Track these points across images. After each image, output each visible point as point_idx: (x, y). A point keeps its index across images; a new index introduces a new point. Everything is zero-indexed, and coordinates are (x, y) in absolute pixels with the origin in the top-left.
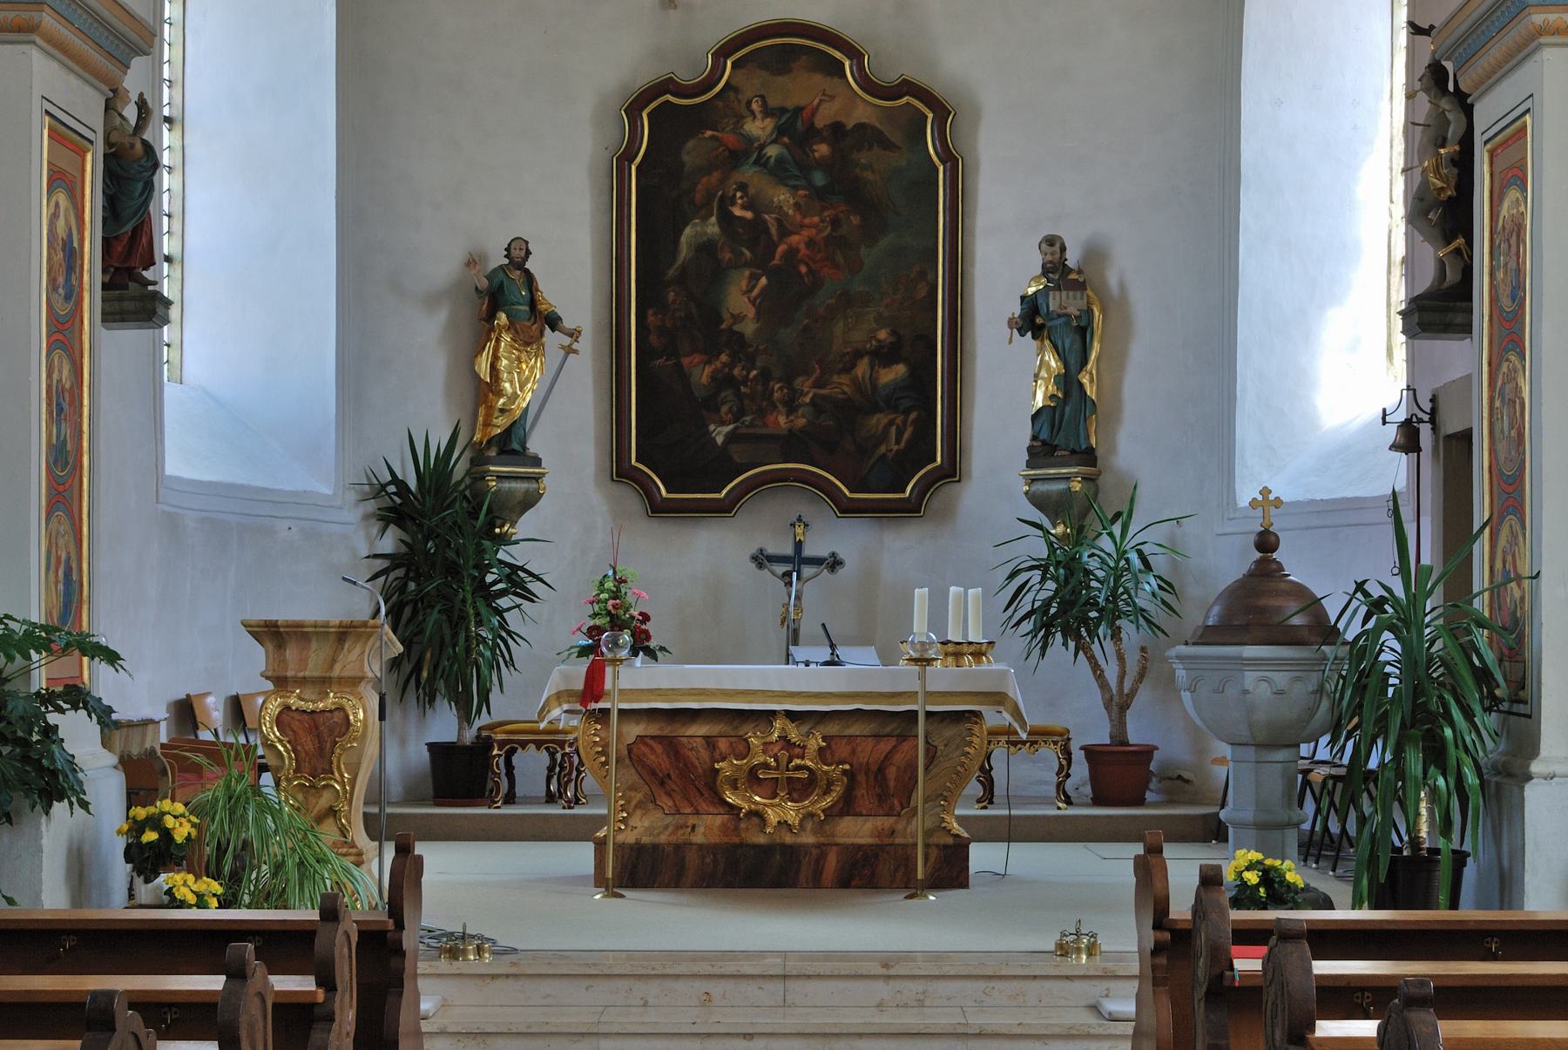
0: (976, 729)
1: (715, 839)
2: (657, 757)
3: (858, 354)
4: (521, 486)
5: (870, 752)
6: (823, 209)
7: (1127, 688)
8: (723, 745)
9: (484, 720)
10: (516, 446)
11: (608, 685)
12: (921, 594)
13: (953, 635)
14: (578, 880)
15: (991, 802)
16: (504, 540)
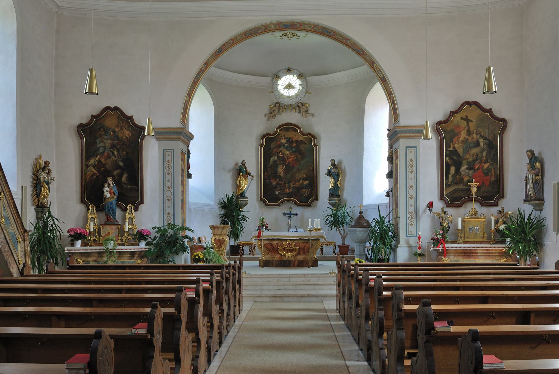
0: (319, 242)
1: (278, 259)
2: (269, 246)
3: (300, 179)
4: (244, 202)
5: (302, 245)
6: (294, 155)
7: (345, 236)
8: (279, 244)
9: (239, 241)
10: (243, 195)
11: (261, 235)
12: (310, 220)
13: (315, 227)
14: (257, 266)
15: (323, 254)
16: (241, 211)
